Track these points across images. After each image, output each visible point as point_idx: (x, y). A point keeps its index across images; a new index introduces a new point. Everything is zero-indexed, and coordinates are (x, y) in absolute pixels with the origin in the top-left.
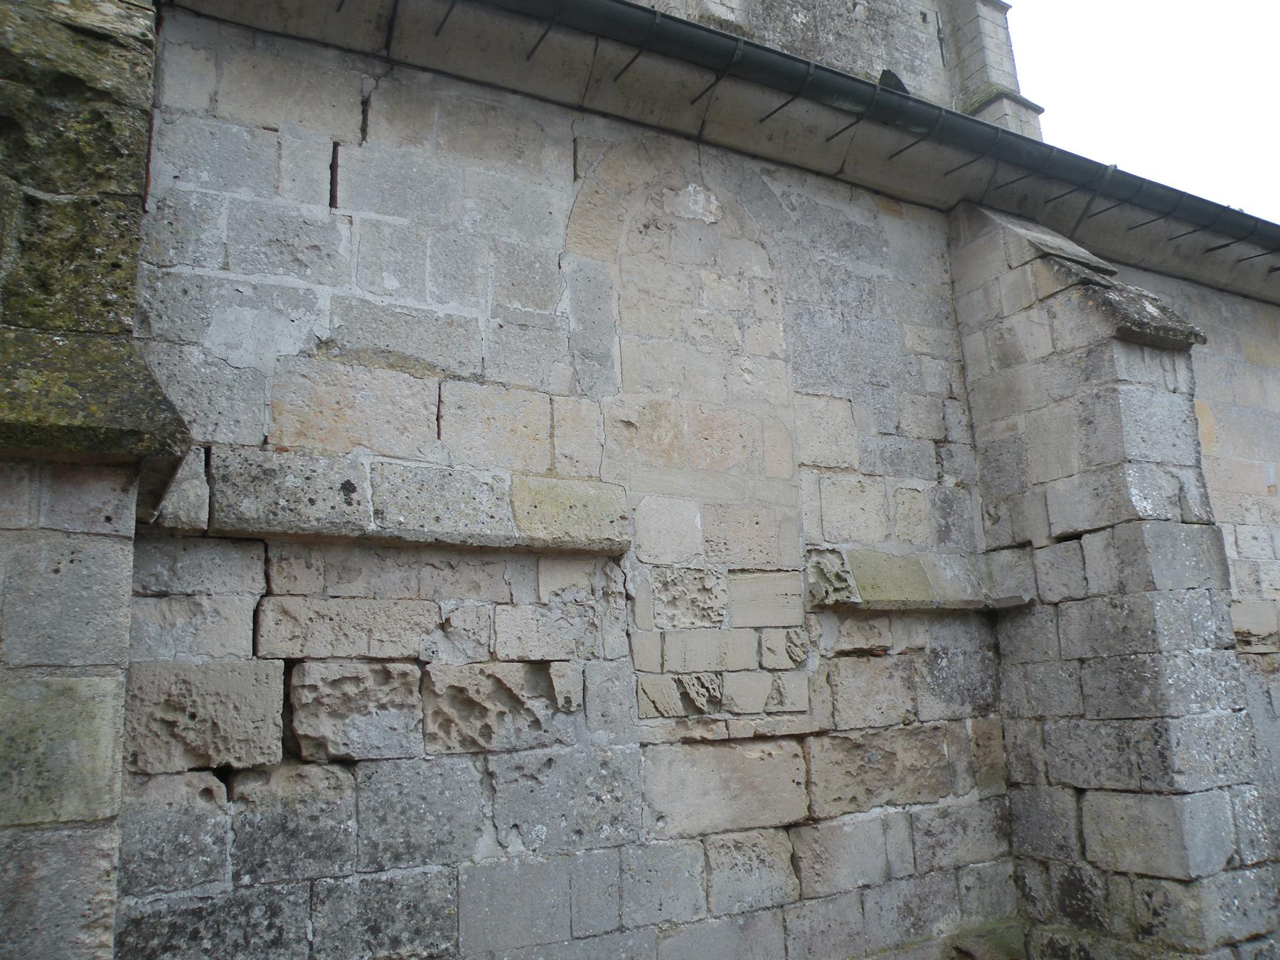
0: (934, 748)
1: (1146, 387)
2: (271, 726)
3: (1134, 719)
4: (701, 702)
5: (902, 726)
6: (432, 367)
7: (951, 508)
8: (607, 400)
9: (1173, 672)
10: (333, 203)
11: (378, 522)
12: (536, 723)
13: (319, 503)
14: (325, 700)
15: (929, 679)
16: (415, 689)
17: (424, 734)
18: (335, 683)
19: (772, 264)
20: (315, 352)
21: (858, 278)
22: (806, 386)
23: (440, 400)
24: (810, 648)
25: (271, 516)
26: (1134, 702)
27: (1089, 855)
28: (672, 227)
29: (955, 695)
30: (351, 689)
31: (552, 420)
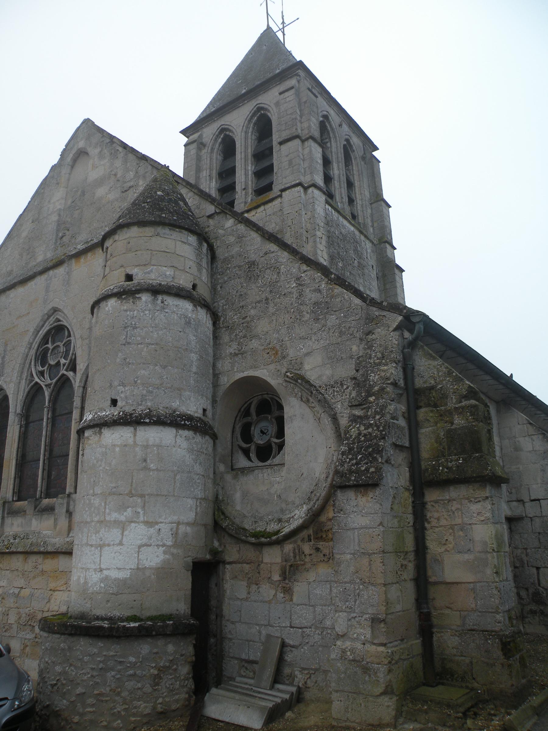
27: (542, 585)
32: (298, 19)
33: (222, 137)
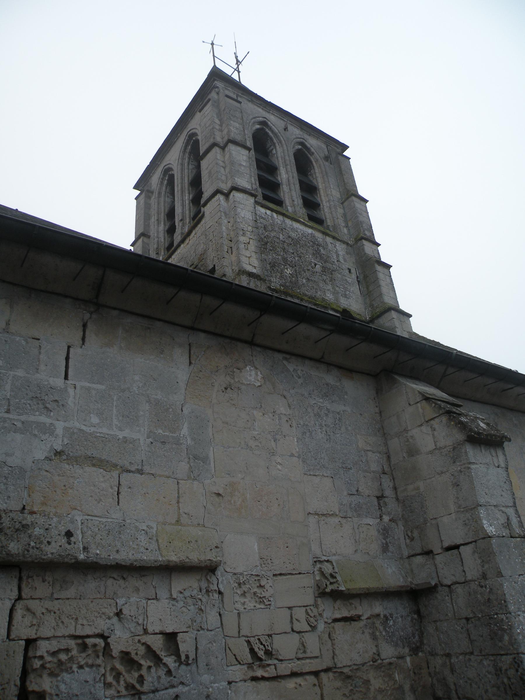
0: (391, 677)
1: (484, 465)
2: (13, 686)
3: (502, 655)
4: (261, 654)
5: (371, 663)
6: (115, 466)
7: (388, 533)
8: (207, 482)
9: (519, 625)
10: (66, 377)
11: (85, 554)
12: (169, 672)
13: (53, 544)
14: (48, 665)
15: (384, 633)
16: (101, 654)
17: (105, 684)
18: (54, 654)
19: (289, 406)
20: (53, 457)
21: (333, 412)
22: (309, 470)
23: (119, 484)
24: (319, 618)
25: (26, 552)
26: (500, 644)
28: (239, 389)
29: (399, 642)
30: (63, 657)
31: (178, 493)
32: (248, 53)
33: (167, 178)
